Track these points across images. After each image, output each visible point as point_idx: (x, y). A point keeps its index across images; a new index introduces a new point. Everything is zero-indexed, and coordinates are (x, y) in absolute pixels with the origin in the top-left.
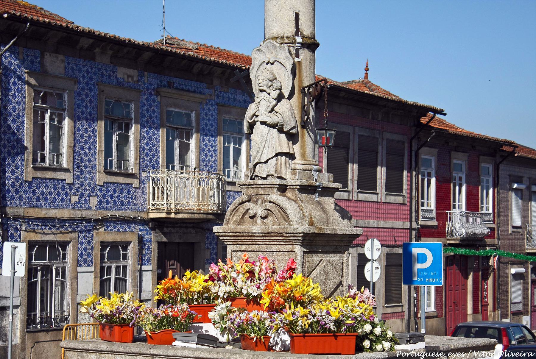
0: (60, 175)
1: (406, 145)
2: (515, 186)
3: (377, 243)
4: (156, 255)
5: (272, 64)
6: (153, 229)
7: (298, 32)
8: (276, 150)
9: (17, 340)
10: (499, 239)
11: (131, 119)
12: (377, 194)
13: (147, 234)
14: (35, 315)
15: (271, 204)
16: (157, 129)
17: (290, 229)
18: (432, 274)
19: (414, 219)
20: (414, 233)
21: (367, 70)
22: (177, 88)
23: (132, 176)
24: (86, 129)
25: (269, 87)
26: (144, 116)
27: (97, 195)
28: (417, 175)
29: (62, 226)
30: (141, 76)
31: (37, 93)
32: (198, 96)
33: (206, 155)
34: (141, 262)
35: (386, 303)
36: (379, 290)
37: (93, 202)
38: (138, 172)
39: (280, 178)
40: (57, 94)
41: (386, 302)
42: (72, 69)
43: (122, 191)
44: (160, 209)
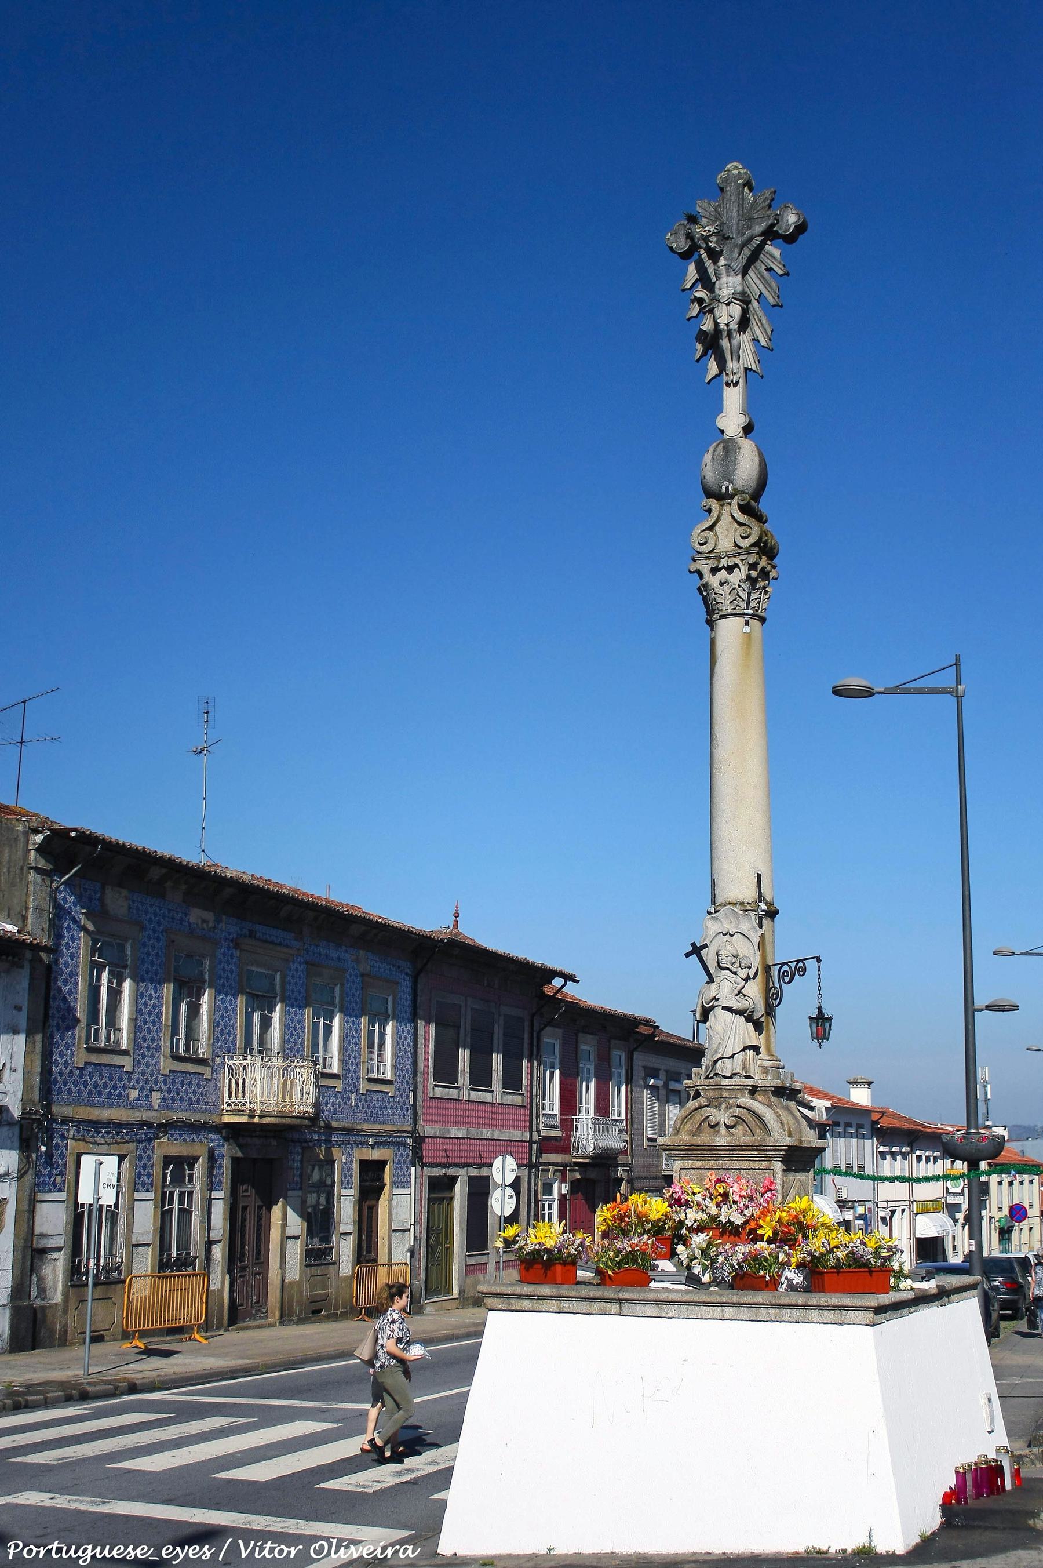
0: (118, 1060)
1: (527, 1023)
2: (652, 1081)
3: (511, 1162)
4: (230, 1176)
5: (732, 935)
6: (226, 1139)
7: (760, 897)
8: (744, 1042)
9: (58, 1298)
10: (632, 1157)
11: (204, 982)
12: (492, 1091)
13: (219, 1146)
14: (80, 1261)
15: (741, 1110)
16: (235, 996)
17: (770, 1142)
19: (534, 1128)
20: (534, 1146)
21: (457, 916)
22: (259, 940)
23: (203, 1062)
24: (151, 995)
25: (733, 964)
26: (220, 978)
27: (160, 1090)
28: (539, 1065)
29: (118, 1133)
30: (218, 921)
31: (95, 942)
32: (285, 950)
33: (292, 1034)
34: (211, 1185)
35: (468, 1250)
36: (493, 1227)
37: (156, 1098)
38: (210, 1057)
40: (119, 944)
42: (138, 909)
43: (190, 1083)
44: (240, 1111)
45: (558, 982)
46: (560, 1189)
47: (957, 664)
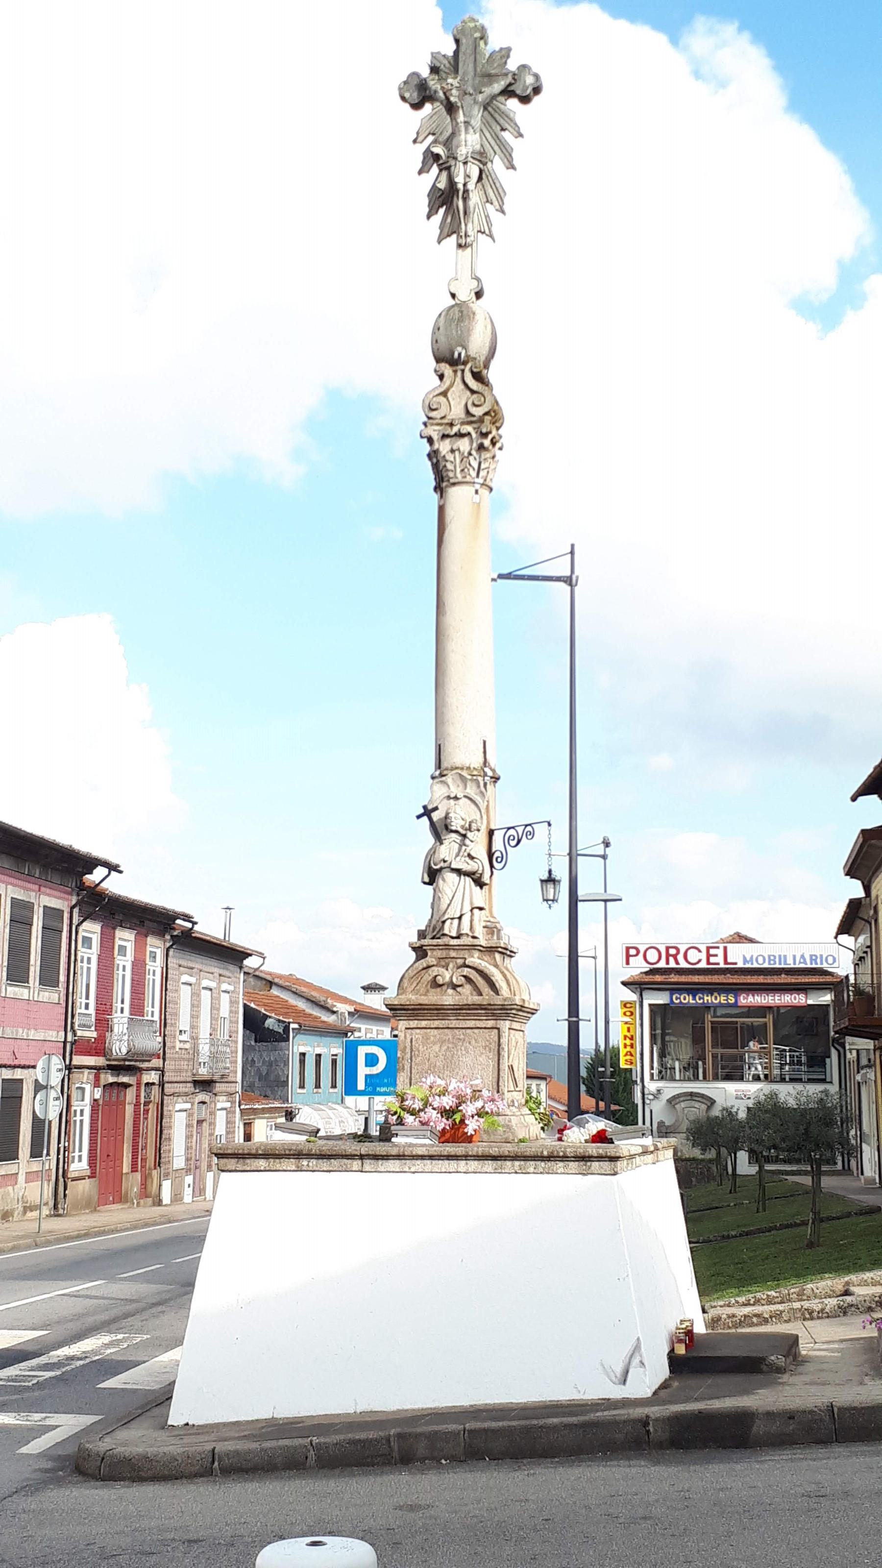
1: (66, 916)
10: (164, 1059)
15: (469, 970)
18: (386, 1081)
39: (474, 937)
41: (32, 1156)
45: (99, 873)
46: (92, 1093)
47: (572, 553)
